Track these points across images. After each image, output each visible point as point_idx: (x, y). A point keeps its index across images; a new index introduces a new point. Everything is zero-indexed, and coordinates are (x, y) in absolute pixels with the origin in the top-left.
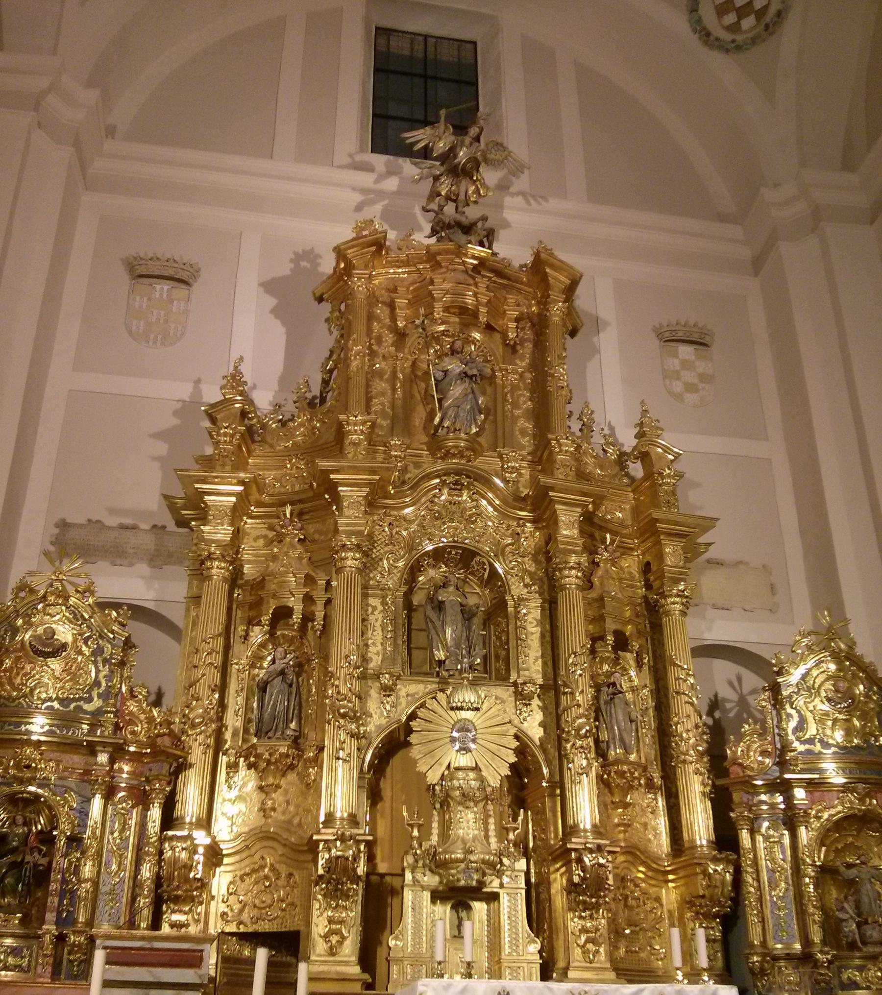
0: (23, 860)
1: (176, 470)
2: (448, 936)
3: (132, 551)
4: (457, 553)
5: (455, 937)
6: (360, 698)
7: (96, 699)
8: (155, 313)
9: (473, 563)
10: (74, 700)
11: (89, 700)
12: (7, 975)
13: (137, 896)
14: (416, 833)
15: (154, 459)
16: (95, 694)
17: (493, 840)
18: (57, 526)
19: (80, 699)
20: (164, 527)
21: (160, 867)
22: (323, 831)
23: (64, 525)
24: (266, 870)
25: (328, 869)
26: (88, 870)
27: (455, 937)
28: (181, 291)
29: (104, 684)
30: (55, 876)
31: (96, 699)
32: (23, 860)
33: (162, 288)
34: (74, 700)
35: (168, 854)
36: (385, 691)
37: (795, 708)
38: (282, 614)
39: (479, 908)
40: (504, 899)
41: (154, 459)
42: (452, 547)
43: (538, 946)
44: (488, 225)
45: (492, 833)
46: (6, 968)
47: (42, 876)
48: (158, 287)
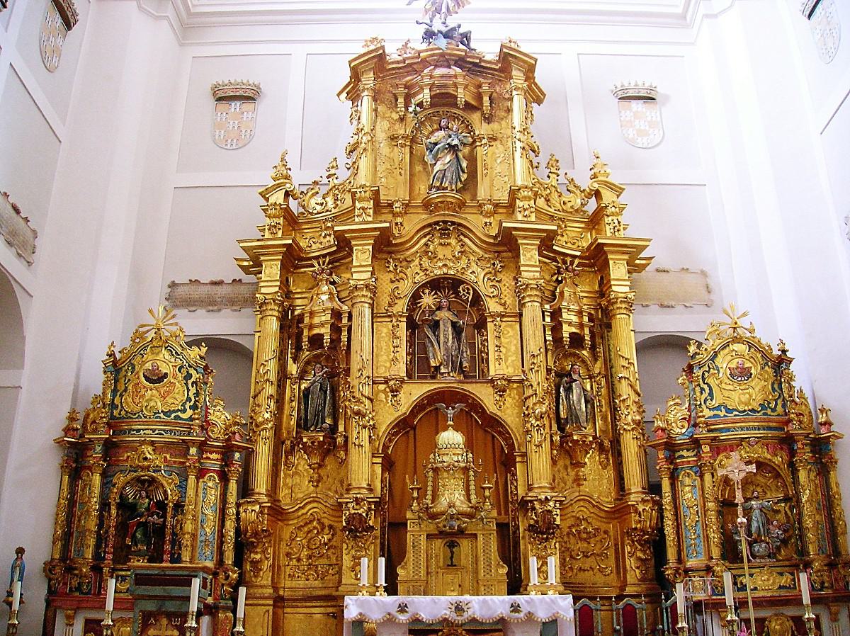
0: (146, 520)
1: (240, 242)
2: (441, 564)
3: (220, 300)
4: (448, 283)
5: (448, 565)
6: (371, 400)
7: (188, 409)
8: (231, 123)
9: (461, 289)
10: (174, 411)
11: (184, 411)
12: (193, 634)
13: (223, 542)
14: (415, 494)
15: (636, 82)
16: (187, 407)
17: (473, 497)
18: (169, 287)
19: (178, 410)
20: (240, 280)
21: (238, 524)
22: (345, 496)
23: (173, 285)
24: (315, 523)
25: (348, 522)
26: (189, 527)
27: (448, 565)
28: (248, 106)
29: (193, 400)
30: (168, 531)
31: (188, 409)
32: (146, 520)
33: (236, 105)
34: (174, 411)
35: (243, 515)
36: (393, 392)
37: (707, 383)
38: (316, 341)
39: (465, 545)
40: (480, 538)
41: (636, 82)
42: (443, 278)
43: (505, 570)
44: (462, 30)
45: (473, 492)
46: (196, 630)
47: (160, 531)
48: (233, 104)
